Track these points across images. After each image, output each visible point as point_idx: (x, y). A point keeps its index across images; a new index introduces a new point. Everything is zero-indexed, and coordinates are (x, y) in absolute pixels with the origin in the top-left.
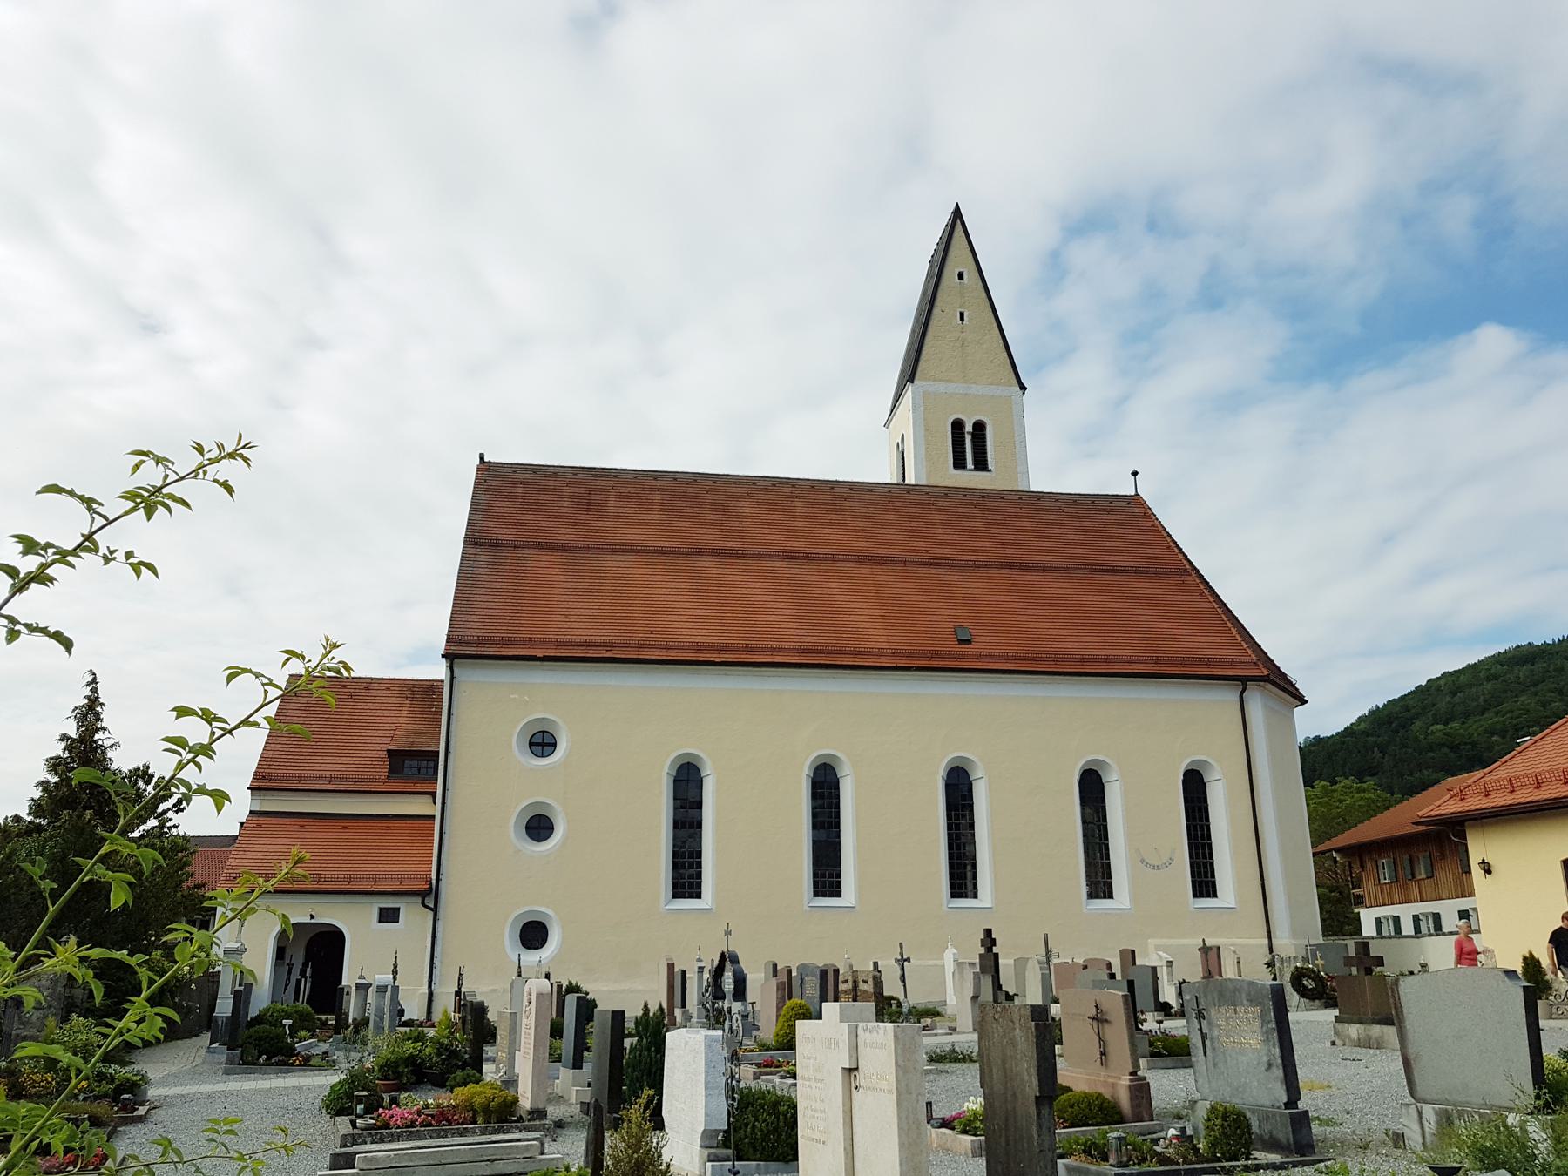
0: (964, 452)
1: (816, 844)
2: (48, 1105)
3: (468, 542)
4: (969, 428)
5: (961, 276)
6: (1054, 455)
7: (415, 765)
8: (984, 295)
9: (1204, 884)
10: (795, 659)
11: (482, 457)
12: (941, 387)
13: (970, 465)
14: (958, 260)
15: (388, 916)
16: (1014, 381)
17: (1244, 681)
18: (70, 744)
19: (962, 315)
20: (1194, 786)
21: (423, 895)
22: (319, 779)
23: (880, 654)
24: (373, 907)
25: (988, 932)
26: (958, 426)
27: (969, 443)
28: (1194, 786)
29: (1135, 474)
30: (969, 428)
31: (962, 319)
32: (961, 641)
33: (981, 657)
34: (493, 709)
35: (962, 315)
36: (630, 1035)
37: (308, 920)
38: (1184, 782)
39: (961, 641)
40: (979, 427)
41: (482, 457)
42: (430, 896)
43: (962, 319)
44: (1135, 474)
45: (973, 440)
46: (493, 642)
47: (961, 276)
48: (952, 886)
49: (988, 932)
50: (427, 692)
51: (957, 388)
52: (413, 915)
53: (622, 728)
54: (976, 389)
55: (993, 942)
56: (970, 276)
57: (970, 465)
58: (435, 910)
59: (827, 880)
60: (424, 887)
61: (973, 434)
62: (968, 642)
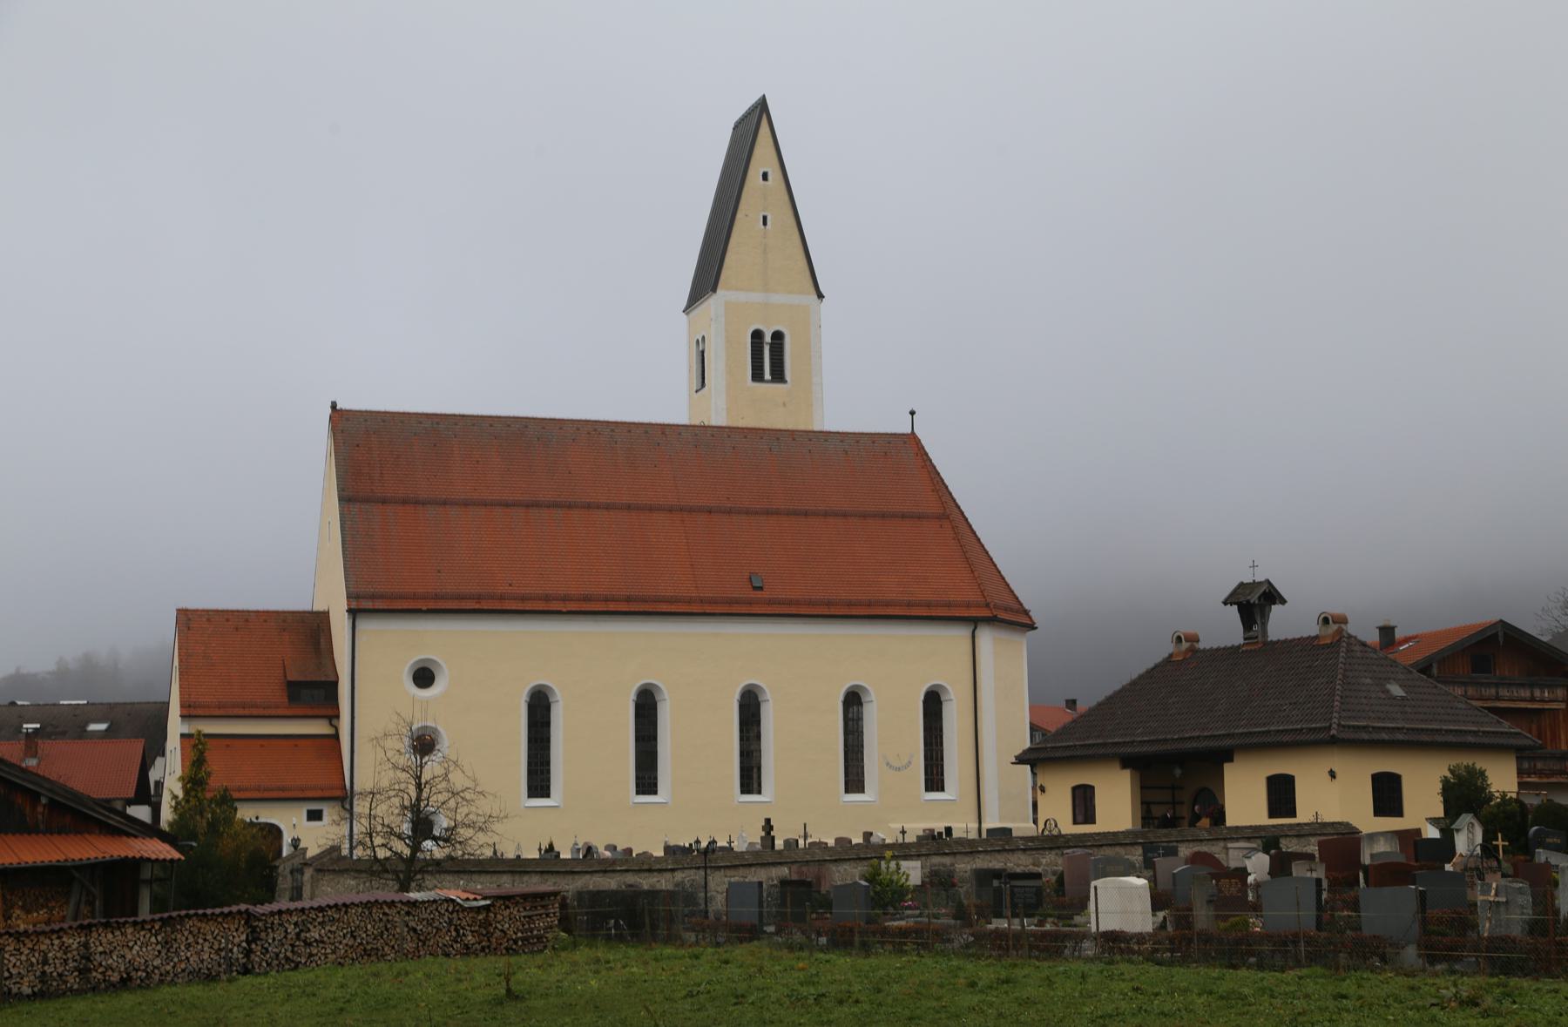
0: (762, 358)
4: (768, 339)
5: (765, 177)
6: (848, 391)
7: (316, 692)
8: (786, 198)
9: (934, 780)
10: (623, 607)
11: (334, 406)
12: (742, 297)
13: (767, 376)
14: (762, 158)
15: (315, 816)
16: (812, 289)
17: (975, 622)
19: (765, 218)
20: (933, 703)
22: (234, 706)
23: (690, 601)
24: (301, 812)
25: (768, 821)
26: (757, 335)
27: (768, 356)
28: (933, 703)
29: (912, 413)
30: (768, 339)
31: (765, 223)
32: (755, 588)
33: (771, 602)
35: (765, 218)
38: (925, 702)
39: (755, 588)
40: (778, 336)
41: (334, 406)
43: (765, 223)
44: (912, 413)
46: (382, 597)
47: (765, 177)
48: (742, 785)
49: (768, 821)
50: (313, 627)
51: (756, 297)
54: (778, 298)
55: (771, 828)
56: (775, 175)
57: (767, 376)
59: (646, 782)
60: (338, 793)
61: (771, 345)
62: (761, 588)
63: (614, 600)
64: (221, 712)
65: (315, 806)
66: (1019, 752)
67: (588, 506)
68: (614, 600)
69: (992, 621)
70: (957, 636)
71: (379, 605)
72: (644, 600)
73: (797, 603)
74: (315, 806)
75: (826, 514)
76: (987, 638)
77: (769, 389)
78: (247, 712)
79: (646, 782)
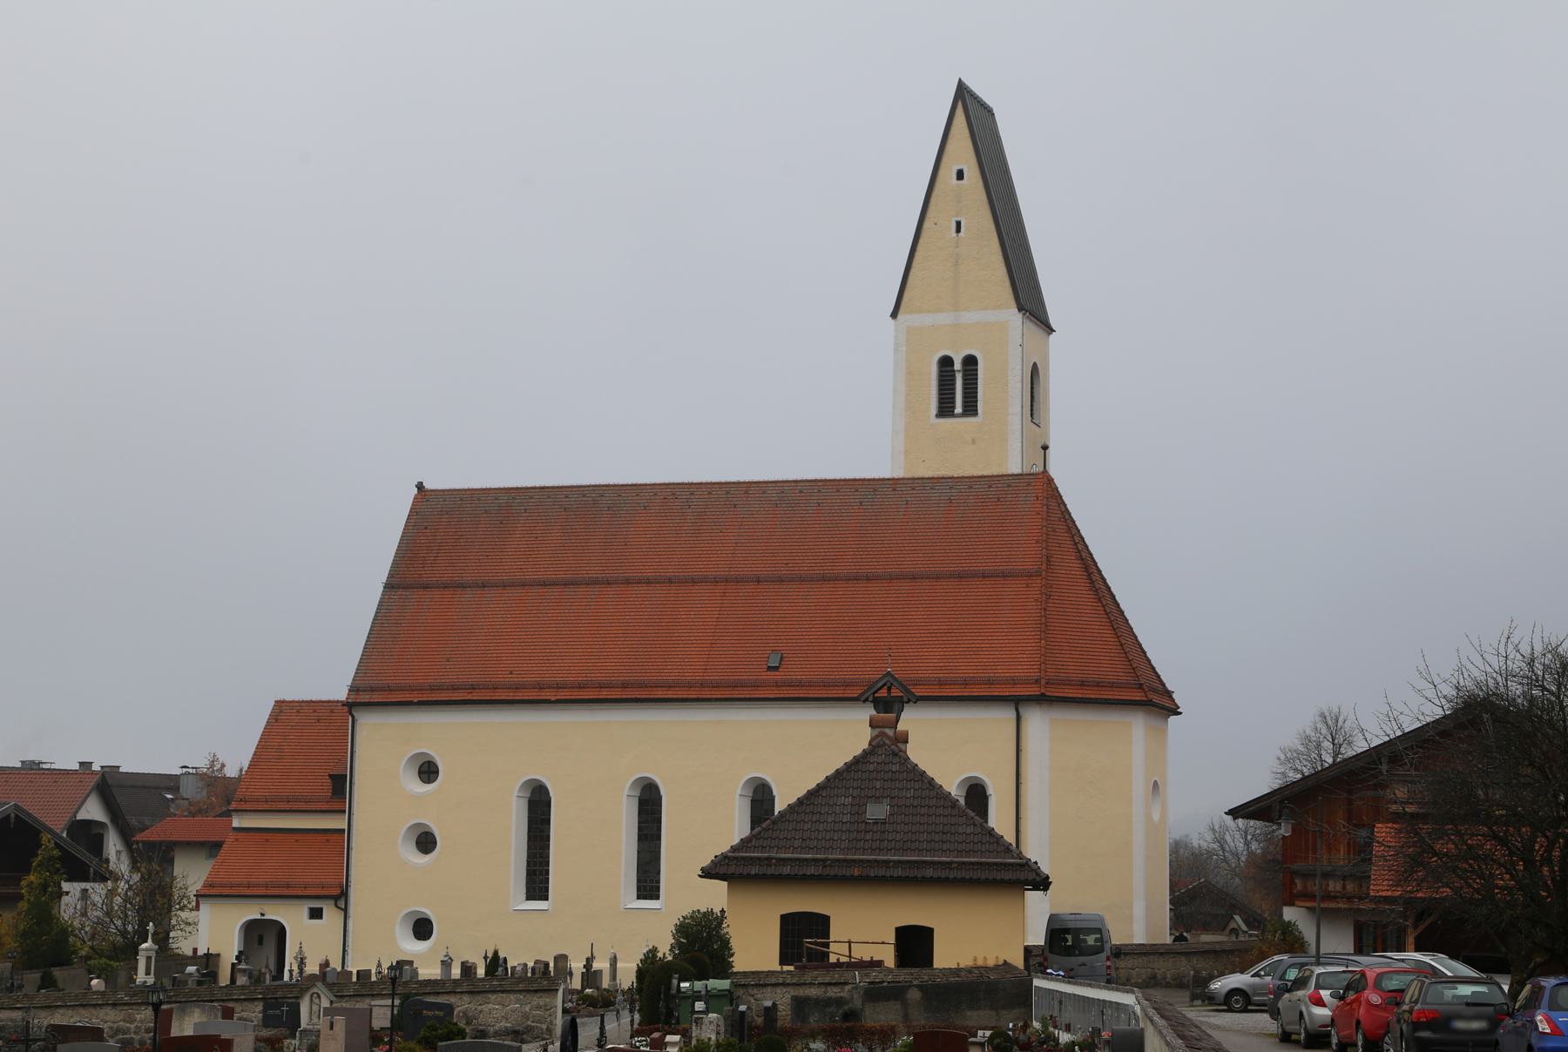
0: (965, 388)
1: (657, 837)
2: (449, 1009)
3: (389, 586)
4: (958, 366)
5: (960, 175)
8: (927, 225)
11: (420, 486)
12: (927, 320)
15: (316, 914)
18: (289, 719)
19: (958, 224)
21: (336, 898)
24: (303, 909)
26: (946, 362)
30: (958, 366)
31: (958, 230)
34: (383, 746)
36: (1344, 887)
37: (258, 917)
40: (970, 361)
42: (341, 897)
43: (958, 230)
44: (1045, 448)
45: (964, 380)
47: (960, 175)
51: (944, 318)
52: (331, 915)
53: (492, 753)
54: (970, 317)
57: (959, 409)
58: (345, 911)
59: (537, 886)
60: (337, 892)
63: (609, 686)
64: (266, 807)
65: (316, 904)
66: (706, 862)
67: (628, 582)
68: (609, 686)
69: (1042, 700)
70: (1002, 717)
71: (376, 698)
72: (642, 685)
73: (810, 685)
74: (316, 904)
75: (892, 578)
76: (1038, 723)
77: (958, 425)
78: (287, 807)
79: (537, 886)
